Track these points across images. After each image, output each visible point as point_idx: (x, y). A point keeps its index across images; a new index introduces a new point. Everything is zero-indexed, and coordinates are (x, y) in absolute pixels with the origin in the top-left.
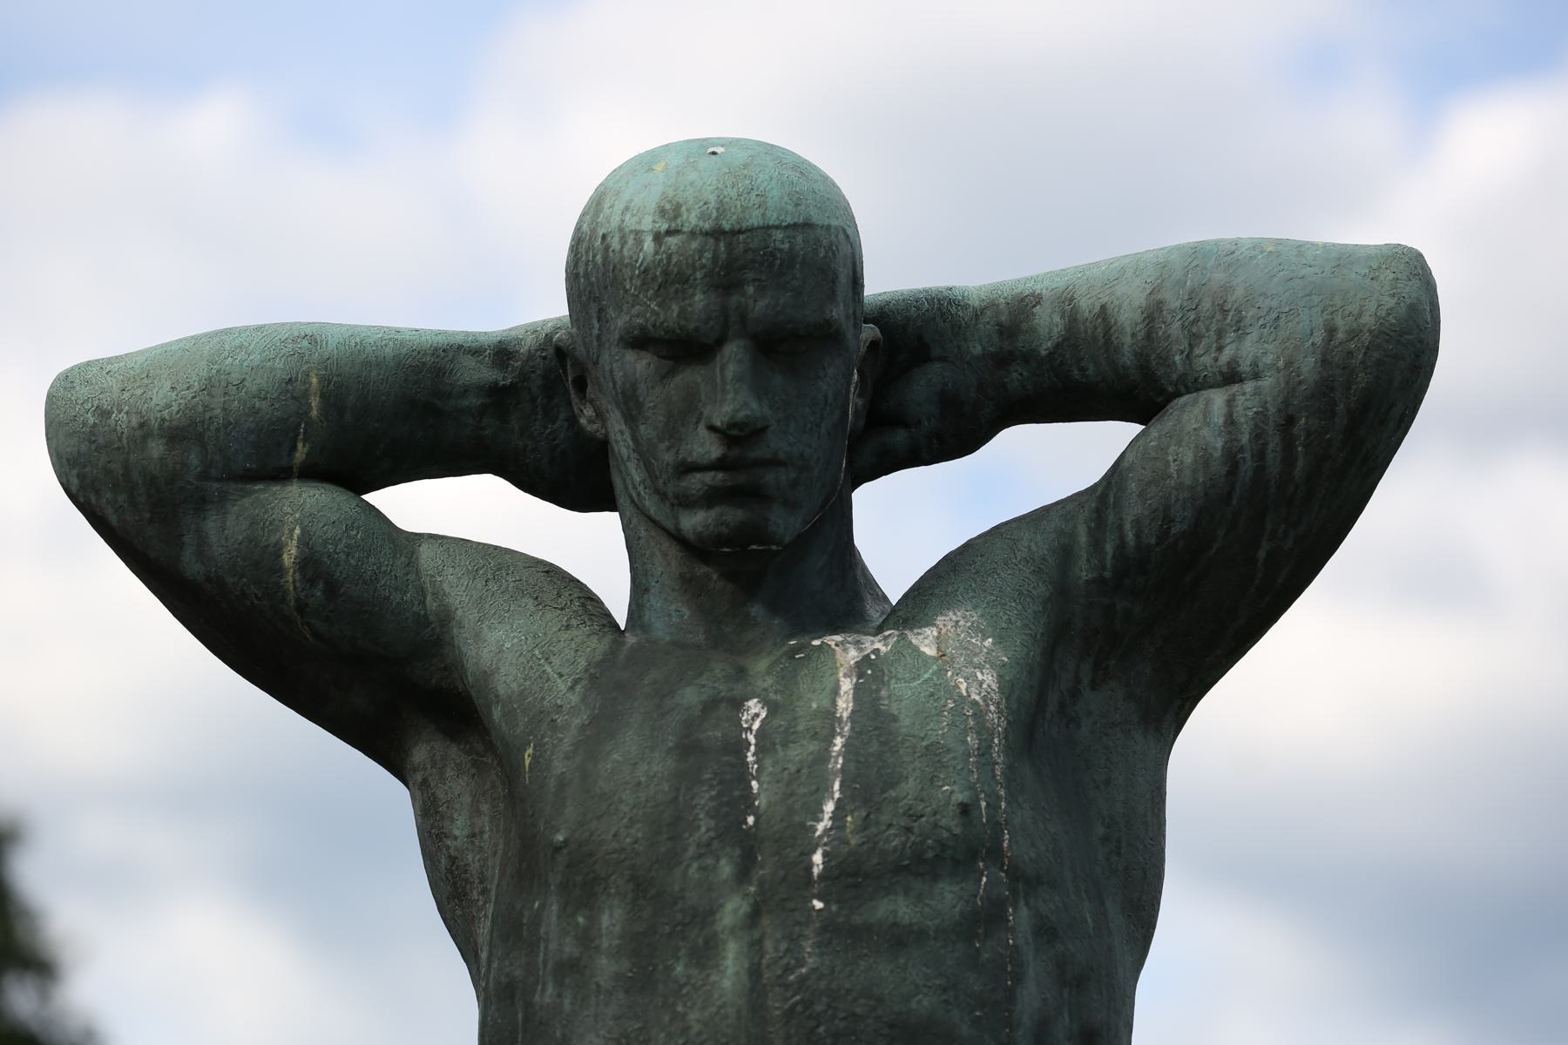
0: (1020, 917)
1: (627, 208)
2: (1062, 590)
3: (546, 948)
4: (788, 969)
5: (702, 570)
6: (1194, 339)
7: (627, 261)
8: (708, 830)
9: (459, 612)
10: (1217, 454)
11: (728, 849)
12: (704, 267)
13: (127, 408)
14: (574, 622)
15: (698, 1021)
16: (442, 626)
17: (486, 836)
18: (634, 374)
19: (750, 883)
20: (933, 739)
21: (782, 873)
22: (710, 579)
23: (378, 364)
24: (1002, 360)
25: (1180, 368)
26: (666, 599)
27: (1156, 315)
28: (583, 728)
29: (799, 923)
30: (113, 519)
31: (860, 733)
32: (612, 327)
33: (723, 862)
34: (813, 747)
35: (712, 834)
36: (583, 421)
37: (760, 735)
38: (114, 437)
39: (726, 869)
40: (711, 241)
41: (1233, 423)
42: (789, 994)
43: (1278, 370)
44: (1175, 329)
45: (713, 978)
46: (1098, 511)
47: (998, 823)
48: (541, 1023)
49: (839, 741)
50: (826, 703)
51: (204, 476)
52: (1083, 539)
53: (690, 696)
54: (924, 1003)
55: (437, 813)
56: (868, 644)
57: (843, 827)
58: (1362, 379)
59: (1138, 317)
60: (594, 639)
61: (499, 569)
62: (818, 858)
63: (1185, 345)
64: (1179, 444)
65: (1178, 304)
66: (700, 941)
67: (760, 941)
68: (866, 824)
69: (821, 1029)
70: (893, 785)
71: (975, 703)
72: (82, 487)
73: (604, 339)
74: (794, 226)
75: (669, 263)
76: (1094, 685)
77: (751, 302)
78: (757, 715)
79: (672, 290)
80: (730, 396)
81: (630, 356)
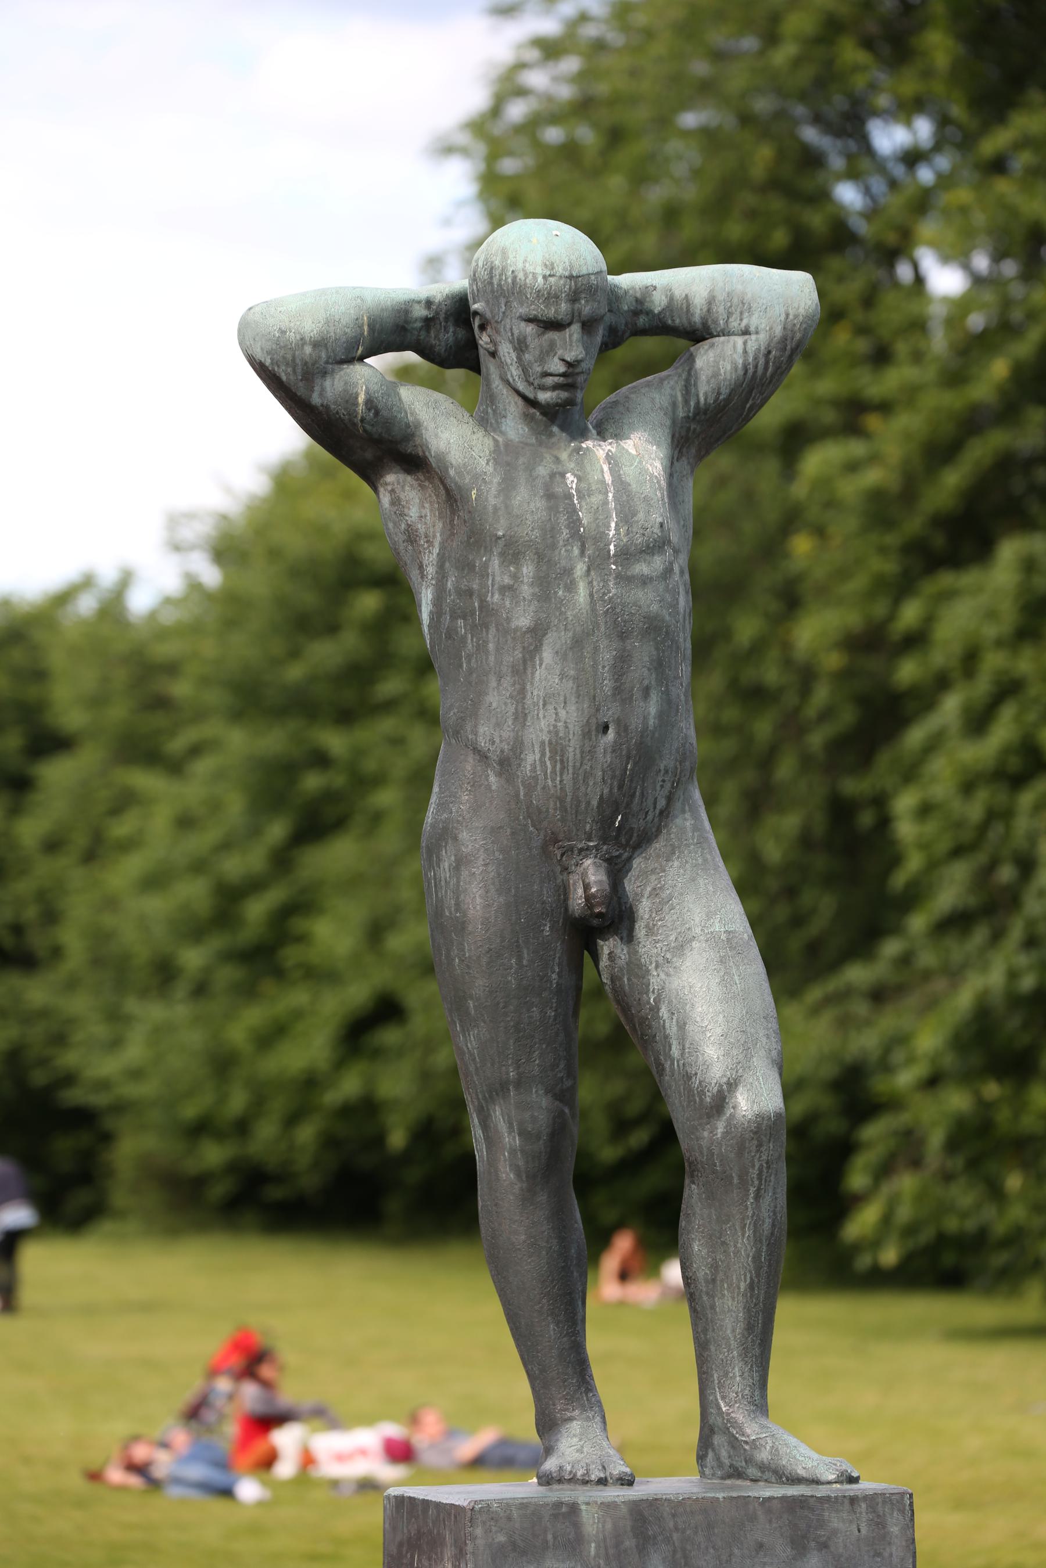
1: (526, 261)
2: (674, 422)
4: (604, 594)
5: (532, 411)
6: (729, 314)
8: (566, 534)
9: (425, 423)
10: (740, 366)
11: (576, 543)
12: (566, 292)
13: (293, 331)
14: (475, 430)
16: (415, 428)
17: (428, 518)
21: (597, 553)
22: (536, 415)
23: (386, 310)
24: (636, 313)
27: (712, 302)
28: (499, 484)
29: (606, 574)
33: (575, 548)
34: (601, 497)
35: (568, 536)
37: (578, 490)
38: (288, 343)
39: (576, 551)
40: (568, 280)
41: (746, 352)
44: (721, 309)
49: (610, 495)
50: (600, 477)
51: (327, 363)
52: (680, 398)
53: (542, 471)
54: (655, 608)
57: (619, 534)
58: (798, 336)
59: (703, 302)
61: (436, 403)
62: (612, 547)
63: (725, 316)
64: (724, 361)
66: (569, 581)
68: (628, 533)
69: (619, 619)
71: (656, 477)
72: (272, 363)
73: (507, 314)
74: (597, 273)
77: (583, 308)
81: (523, 324)
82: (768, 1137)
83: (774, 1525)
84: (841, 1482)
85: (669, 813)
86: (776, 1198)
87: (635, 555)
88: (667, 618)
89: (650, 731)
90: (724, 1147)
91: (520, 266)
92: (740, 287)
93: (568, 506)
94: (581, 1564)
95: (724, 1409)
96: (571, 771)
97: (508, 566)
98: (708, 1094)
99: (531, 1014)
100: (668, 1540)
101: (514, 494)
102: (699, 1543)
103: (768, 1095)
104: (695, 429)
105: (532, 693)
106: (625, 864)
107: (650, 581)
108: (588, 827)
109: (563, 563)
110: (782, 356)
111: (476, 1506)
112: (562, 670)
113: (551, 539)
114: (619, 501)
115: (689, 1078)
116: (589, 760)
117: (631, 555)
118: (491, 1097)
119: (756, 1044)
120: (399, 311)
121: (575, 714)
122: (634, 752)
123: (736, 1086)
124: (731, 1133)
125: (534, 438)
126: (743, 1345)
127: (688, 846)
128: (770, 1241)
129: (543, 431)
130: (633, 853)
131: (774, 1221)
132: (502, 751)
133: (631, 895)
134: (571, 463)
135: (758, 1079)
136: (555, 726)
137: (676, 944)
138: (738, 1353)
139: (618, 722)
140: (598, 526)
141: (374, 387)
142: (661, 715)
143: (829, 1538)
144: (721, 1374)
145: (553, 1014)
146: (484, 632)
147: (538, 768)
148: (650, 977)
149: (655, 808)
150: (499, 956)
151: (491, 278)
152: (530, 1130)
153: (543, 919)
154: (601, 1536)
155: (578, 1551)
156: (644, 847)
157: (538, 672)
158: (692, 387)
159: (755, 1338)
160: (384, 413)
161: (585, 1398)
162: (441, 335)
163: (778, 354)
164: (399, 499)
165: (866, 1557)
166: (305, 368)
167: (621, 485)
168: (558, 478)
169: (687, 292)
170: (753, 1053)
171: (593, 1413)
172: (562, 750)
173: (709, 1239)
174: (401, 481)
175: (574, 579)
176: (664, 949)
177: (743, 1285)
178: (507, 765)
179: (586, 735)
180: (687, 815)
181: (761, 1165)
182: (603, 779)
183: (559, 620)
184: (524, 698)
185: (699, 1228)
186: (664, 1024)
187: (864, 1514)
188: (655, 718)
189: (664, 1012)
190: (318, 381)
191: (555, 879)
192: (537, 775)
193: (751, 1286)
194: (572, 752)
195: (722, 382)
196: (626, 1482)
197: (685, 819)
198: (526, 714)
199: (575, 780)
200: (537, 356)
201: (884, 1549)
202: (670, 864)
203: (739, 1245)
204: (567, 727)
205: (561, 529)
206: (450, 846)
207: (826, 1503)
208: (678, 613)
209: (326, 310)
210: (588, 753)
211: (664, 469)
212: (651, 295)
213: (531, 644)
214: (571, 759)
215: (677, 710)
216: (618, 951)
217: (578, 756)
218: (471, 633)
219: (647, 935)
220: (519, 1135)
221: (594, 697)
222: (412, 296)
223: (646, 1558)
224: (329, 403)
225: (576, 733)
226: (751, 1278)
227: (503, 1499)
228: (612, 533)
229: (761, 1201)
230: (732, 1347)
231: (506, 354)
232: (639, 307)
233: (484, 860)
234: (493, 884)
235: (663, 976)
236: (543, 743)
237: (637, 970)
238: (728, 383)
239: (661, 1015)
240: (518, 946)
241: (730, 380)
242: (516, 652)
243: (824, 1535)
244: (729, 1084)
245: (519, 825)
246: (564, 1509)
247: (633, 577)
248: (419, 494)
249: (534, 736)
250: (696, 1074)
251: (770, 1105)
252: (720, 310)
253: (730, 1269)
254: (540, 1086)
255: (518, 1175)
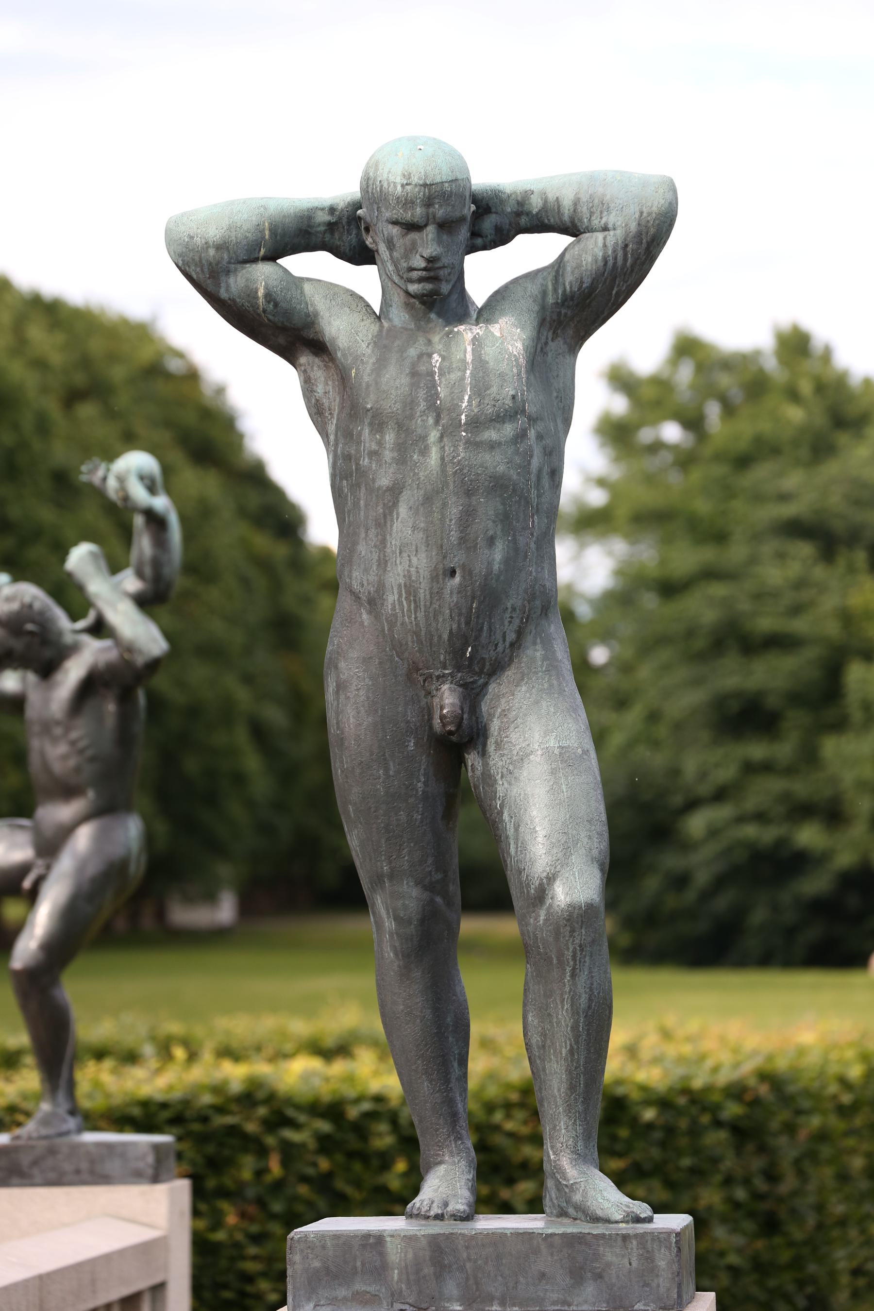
0: (532, 434)
1: (390, 172)
2: (543, 307)
3: (364, 445)
4: (454, 457)
6: (592, 214)
7: (390, 193)
9: (322, 313)
10: (600, 258)
11: (431, 413)
12: (420, 198)
14: (365, 318)
15: (423, 476)
17: (331, 393)
18: (392, 233)
19: (439, 426)
20: (502, 370)
21: (450, 422)
22: (416, 304)
23: (288, 216)
24: (518, 214)
25: (586, 224)
26: (399, 311)
28: (374, 364)
29: (457, 441)
30: (195, 277)
31: (476, 368)
32: (383, 215)
33: (430, 418)
34: (459, 374)
35: (425, 407)
36: (367, 243)
37: (440, 369)
39: (431, 421)
41: (606, 246)
42: (454, 466)
43: (622, 228)
45: (427, 461)
46: (556, 277)
47: (524, 400)
48: (363, 472)
49: (468, 372)
50: (462, 356)
51: (229, 263)
52: (550, 287)
53: (413, 352)
54: (501, 468)
55: (310, 382)
56: (474, 330)
57: (471, 406)
58: (652, 231)
59: (571, 203)
60: (373, 325)
62: (463, 417)
64: (586, 254)
65: (586, 200)
67: (443, 447)
69: (466, 479)
70: (488, 389)
71: (515, 356)
72: (183, 264)
74: (452, 181)
75: (407, 196)
76: (553, 340)
78: (438, 361)
79: (408, 206)
80: (430, 246)
81: (390, 226)
82: (580, 924)
83: (555, 1258)
84: (627, 1222)
85: (520, 645)
86: (592, 977)
87: (485, 423)
88: (515, 477)
89: (495, 574)
90: (545, 932)
91: (385, 176)
92: (601, 190)
93: (429, 382)
94: (386, 1287)
95: (552, 1157)
96: (423, 610)
97: (375, 435)
98: (532, 886)
99: (400, 817)
100: (462, 1269)
101: (385, 372)
102: (489, 1272)
103: (581, 888)
104: (566, 314)
105: (391, 543)
106: (483, 689)
107: (498, 445)
108: (442, 657)
109: (419, 431)
110: (639, 249)
111: (295, 1236)
112: (415, 523)
113: (410, 411)
114: (475, 377)
115: (520, 873)
116: (437, 600)
117: (480, 423)
118: (372, 887)
119: (577, 844)
120: (302, 217)
121: (425, 561)
122: (479, 593)
123: (554, 880)
124: (549, 920)
125: (413, 323)
126: (567, 1102)
127: (536, 673)
128: (587, 1013)
129: (422, 318)
130: (489, 679)
131: (590, 996)
132: (369, 593)
133: (485, 715)
134: (440, 345)
135: (574, 874)
136: (409, 571)
137: (517, 758)
138: (563, 1109)
139: (463, 567)
140: (453, 399)
141: (272, 283)
142: (507, 561)
143: (603, 1270)
144: (551, 1127)
145: (420, 817)
146: (358, 491)
147: (397, 607)
148: (497, 786)
149: (504, 641)
150: (369, 768)
151: (368, 187)
152: (402, 916)
153: (407, 736)
154: (403, 1264)
155: (383, 1276)
156: (498, 674)
157: (395, 525)
158: (561, 277)
159: (577, 1097)
160: (283, 305)
161: (453, 1146)
162: (345, 238)
163: (635, 247)
164: (309, 378)
165: (636, 1287)
166: (210, 267)
167: (480, 362)
168: (425, 358)
169: (558, 195)
170: (572, 852)
171: (459, 1158)
172: (414, 592)
173: (539, 1011)
174: (310, 362)
175: (428, 445)
176: (508, 761)
177: (564, 1051)
178: (374, 603)
179: (434, 578)
180: (539, 647)
181: (575, 948)
182: (451, 616)
183: (413, 480)
184: (385, 547)
185: (532, 1001)
186: (506, 826)
187: (635, 1249)
188: (500, 564)
189: (506, 816)
190: (223, 278)
191: (419, 701)
192: (397, 613)
193: (571, 1052)
194: (423, 592)
195: (584, 272)
196: (459, 1218)
197: (536, 650)
198: (386, 561)
199: (427, 617)
200: (402, 253)
201: (652, 1280)
202: (519, 688)
203: (560, 1017)
204: (418, 572)
205: (419, 402)
206: (333, 675)
207: (601, 1240)
208: (529, 473)
209: (230, 218)
210: (436, 594)
211: (526, 349)
212: (529, 199)
213: (390, 501)
214: (422, 599)
215: (526, 556)
216: (476, 763)
217: (428, 597)
218: (350, 492)
219: (495, 750)
220: (394, 921)
221: (442, 546)
222: (316, 204)
223: (443, 1283)
224: (235, 297)
225: (425, 576)
226: (571, 1045)
227: (320, 1231)
228: (464, 405)
229: (577, 979)
230: (558, 1104)
231: (383, 252)
232: (520, 209)
233: (356, 686)
234: (363, 706)
235: (506, 785)
236: (400, 585)
237: (488, 778)
238: (589, 273)
239: (504, 818)
240: (385, 759)
241: (591, 271)
242: (379, 508)
243: (599, 1267)
244: (548, 878)
245: (386, 656)
246: (371, 1241)
247: (481, 442)
248: (325, 374)
249: (393, 579)
250: (524, 869)
251: (581, 897)
252: (584, 210)
253: (554, 1037)
254: (410, 879)
255: (396, 954)
